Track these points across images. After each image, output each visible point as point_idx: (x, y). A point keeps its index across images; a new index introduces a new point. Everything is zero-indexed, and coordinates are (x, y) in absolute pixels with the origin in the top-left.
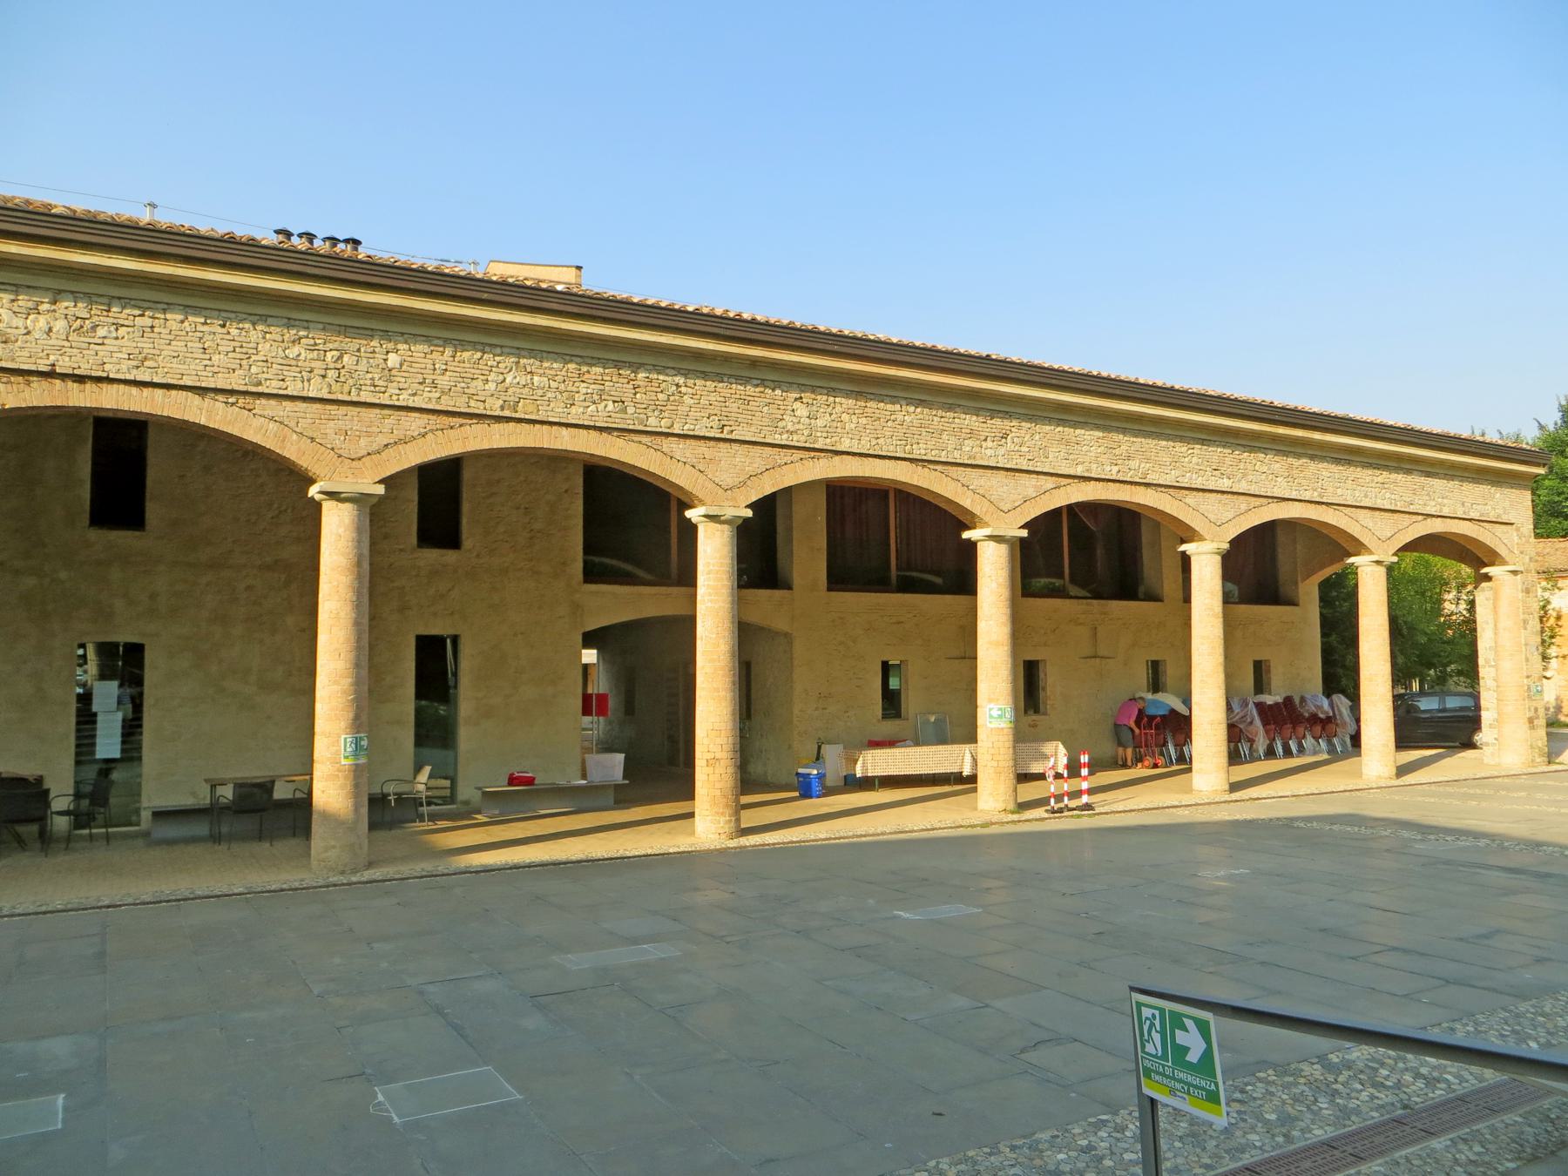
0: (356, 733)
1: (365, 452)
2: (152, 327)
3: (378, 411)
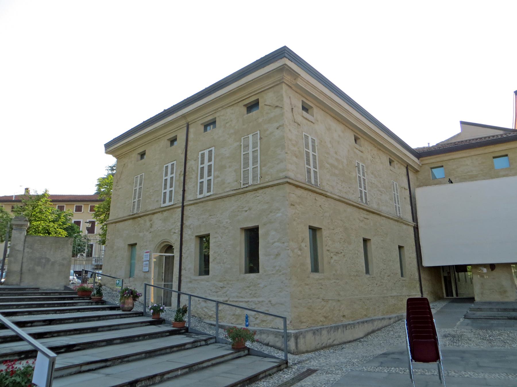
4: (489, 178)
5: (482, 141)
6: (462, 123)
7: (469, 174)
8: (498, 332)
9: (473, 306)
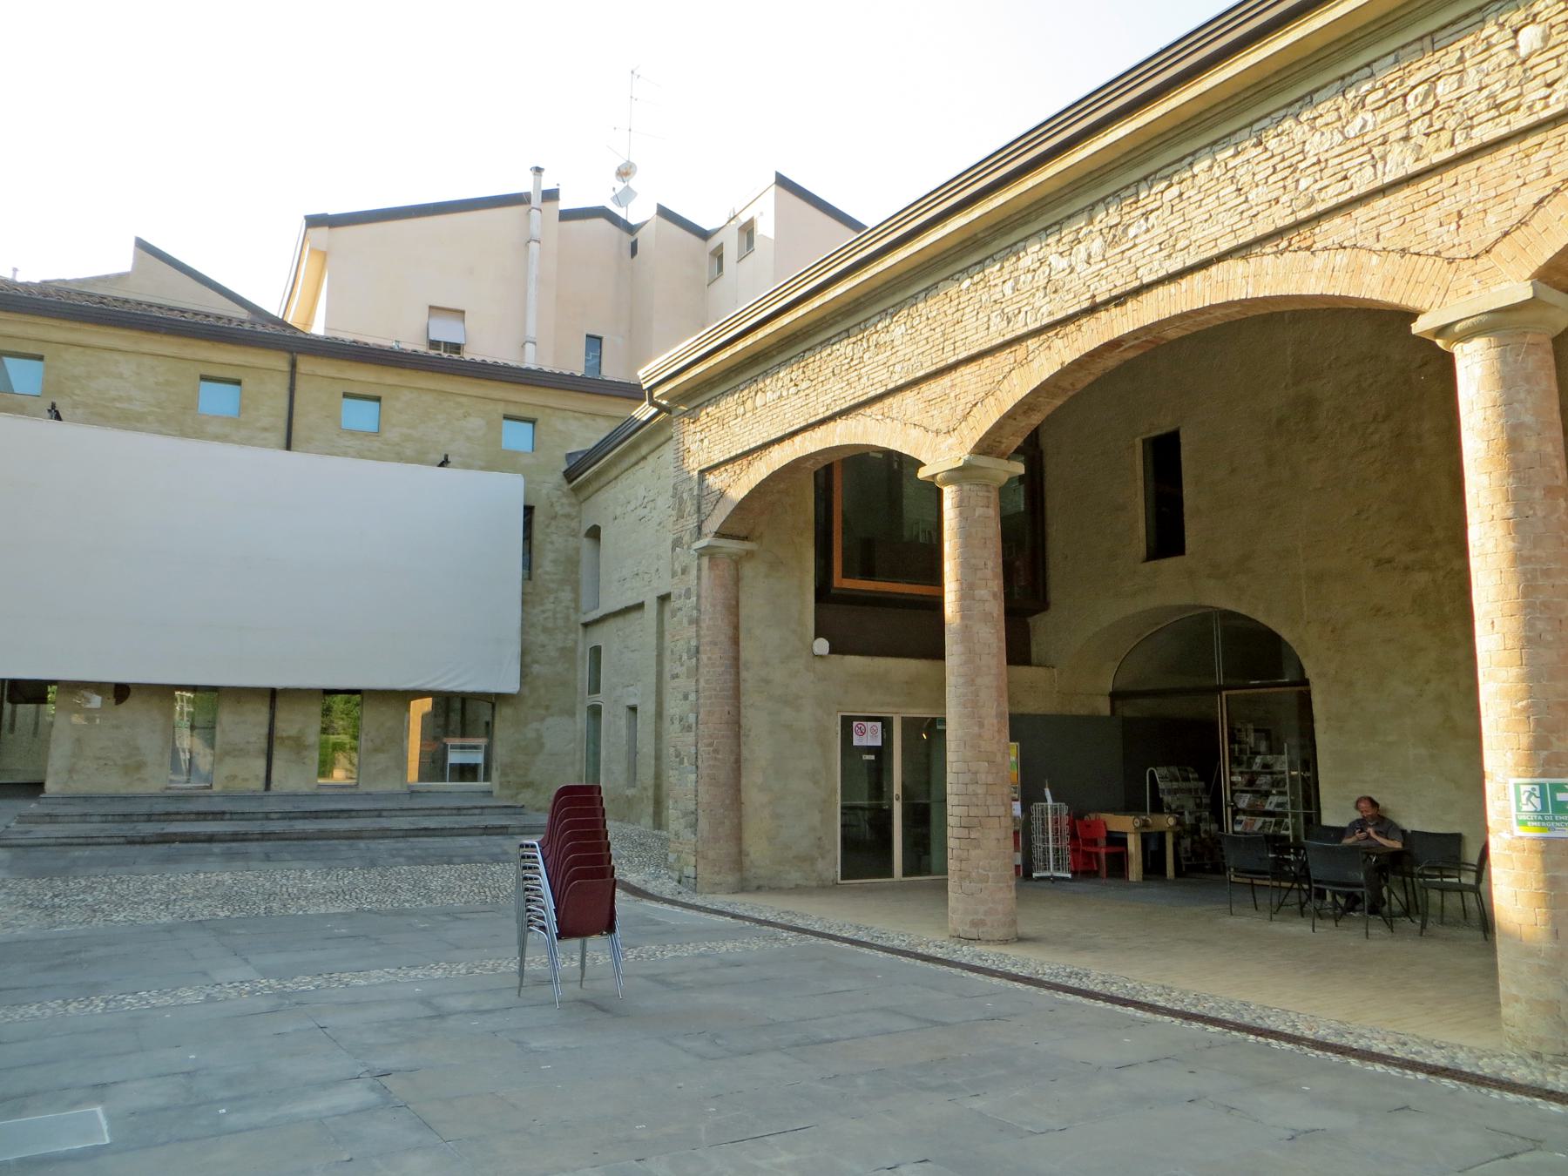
0: (1543, 775)
1: (1498, 234)
2: (1181, 194)
3: (1513, 148)
4: (174, 433)
5: (183, 319)
6: (142, 245)
7: (118, 405)
8: (83, 883)
9: (33, 807)
